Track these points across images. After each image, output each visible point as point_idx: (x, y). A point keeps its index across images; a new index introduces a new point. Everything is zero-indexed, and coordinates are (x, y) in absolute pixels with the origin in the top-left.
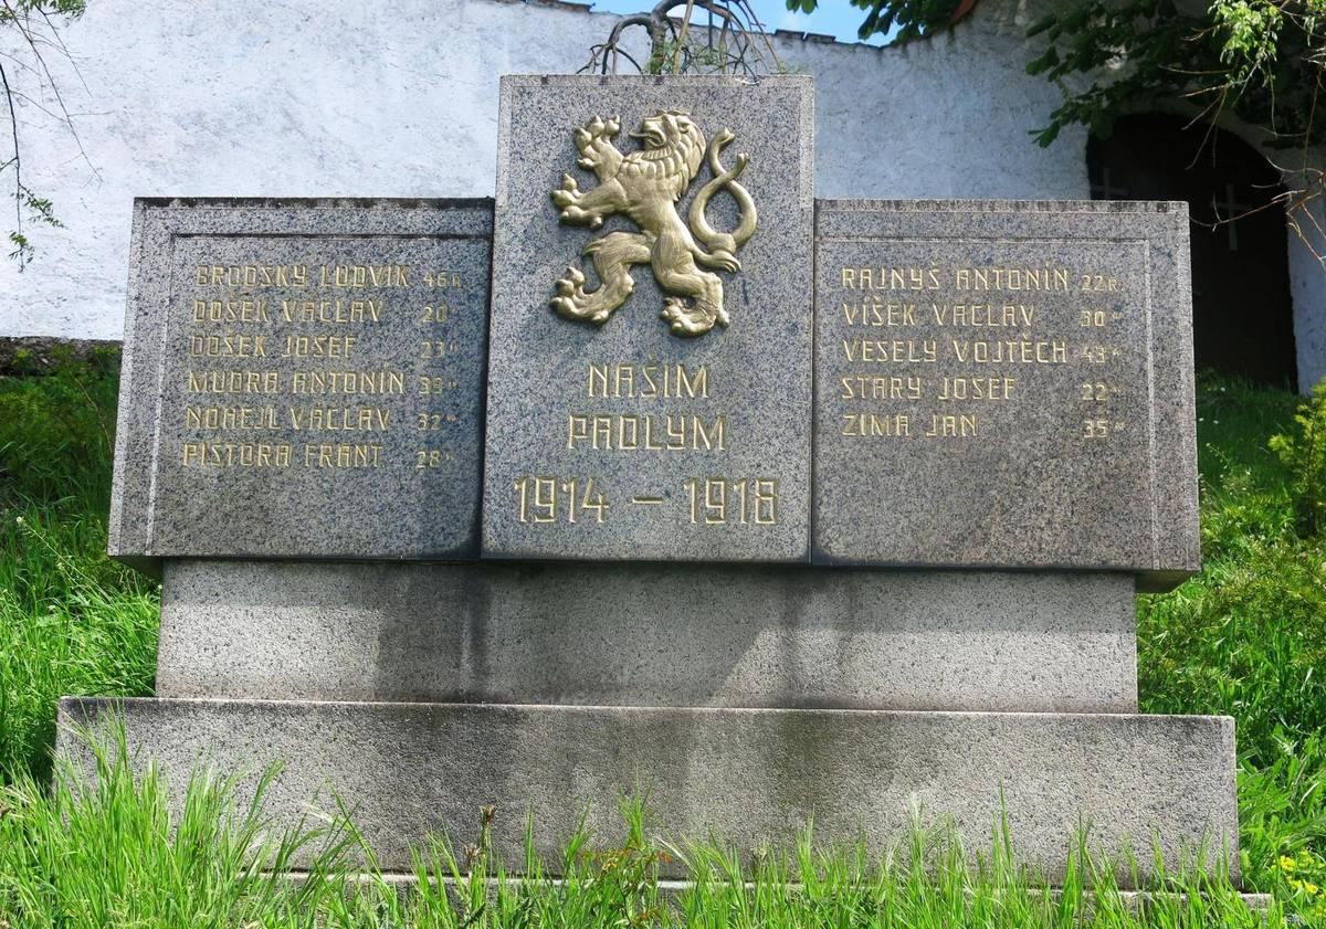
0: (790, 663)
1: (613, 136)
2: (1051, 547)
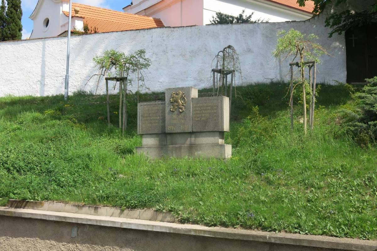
0: (191, 141)
1: (175, 94)
2: (212, 129)
